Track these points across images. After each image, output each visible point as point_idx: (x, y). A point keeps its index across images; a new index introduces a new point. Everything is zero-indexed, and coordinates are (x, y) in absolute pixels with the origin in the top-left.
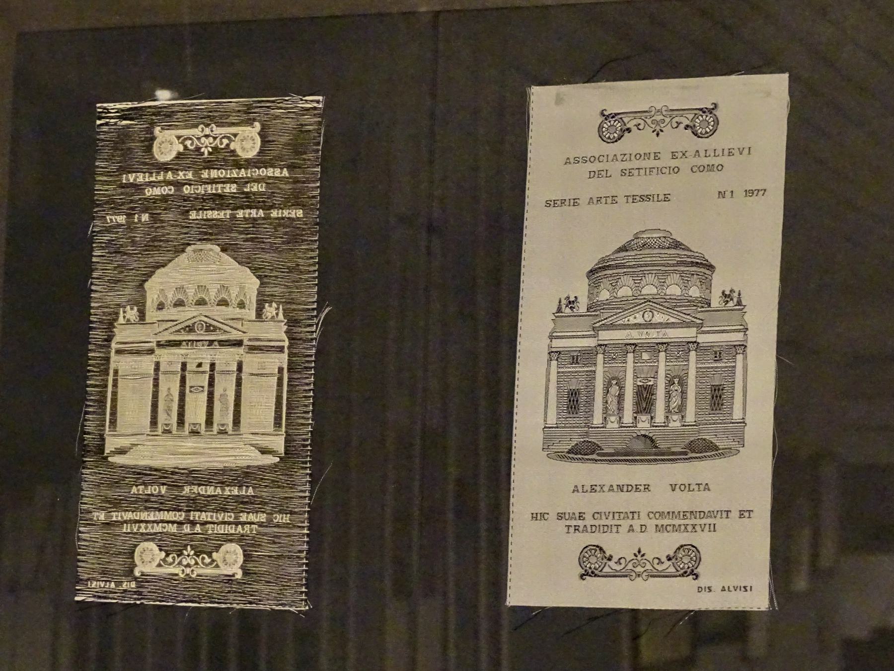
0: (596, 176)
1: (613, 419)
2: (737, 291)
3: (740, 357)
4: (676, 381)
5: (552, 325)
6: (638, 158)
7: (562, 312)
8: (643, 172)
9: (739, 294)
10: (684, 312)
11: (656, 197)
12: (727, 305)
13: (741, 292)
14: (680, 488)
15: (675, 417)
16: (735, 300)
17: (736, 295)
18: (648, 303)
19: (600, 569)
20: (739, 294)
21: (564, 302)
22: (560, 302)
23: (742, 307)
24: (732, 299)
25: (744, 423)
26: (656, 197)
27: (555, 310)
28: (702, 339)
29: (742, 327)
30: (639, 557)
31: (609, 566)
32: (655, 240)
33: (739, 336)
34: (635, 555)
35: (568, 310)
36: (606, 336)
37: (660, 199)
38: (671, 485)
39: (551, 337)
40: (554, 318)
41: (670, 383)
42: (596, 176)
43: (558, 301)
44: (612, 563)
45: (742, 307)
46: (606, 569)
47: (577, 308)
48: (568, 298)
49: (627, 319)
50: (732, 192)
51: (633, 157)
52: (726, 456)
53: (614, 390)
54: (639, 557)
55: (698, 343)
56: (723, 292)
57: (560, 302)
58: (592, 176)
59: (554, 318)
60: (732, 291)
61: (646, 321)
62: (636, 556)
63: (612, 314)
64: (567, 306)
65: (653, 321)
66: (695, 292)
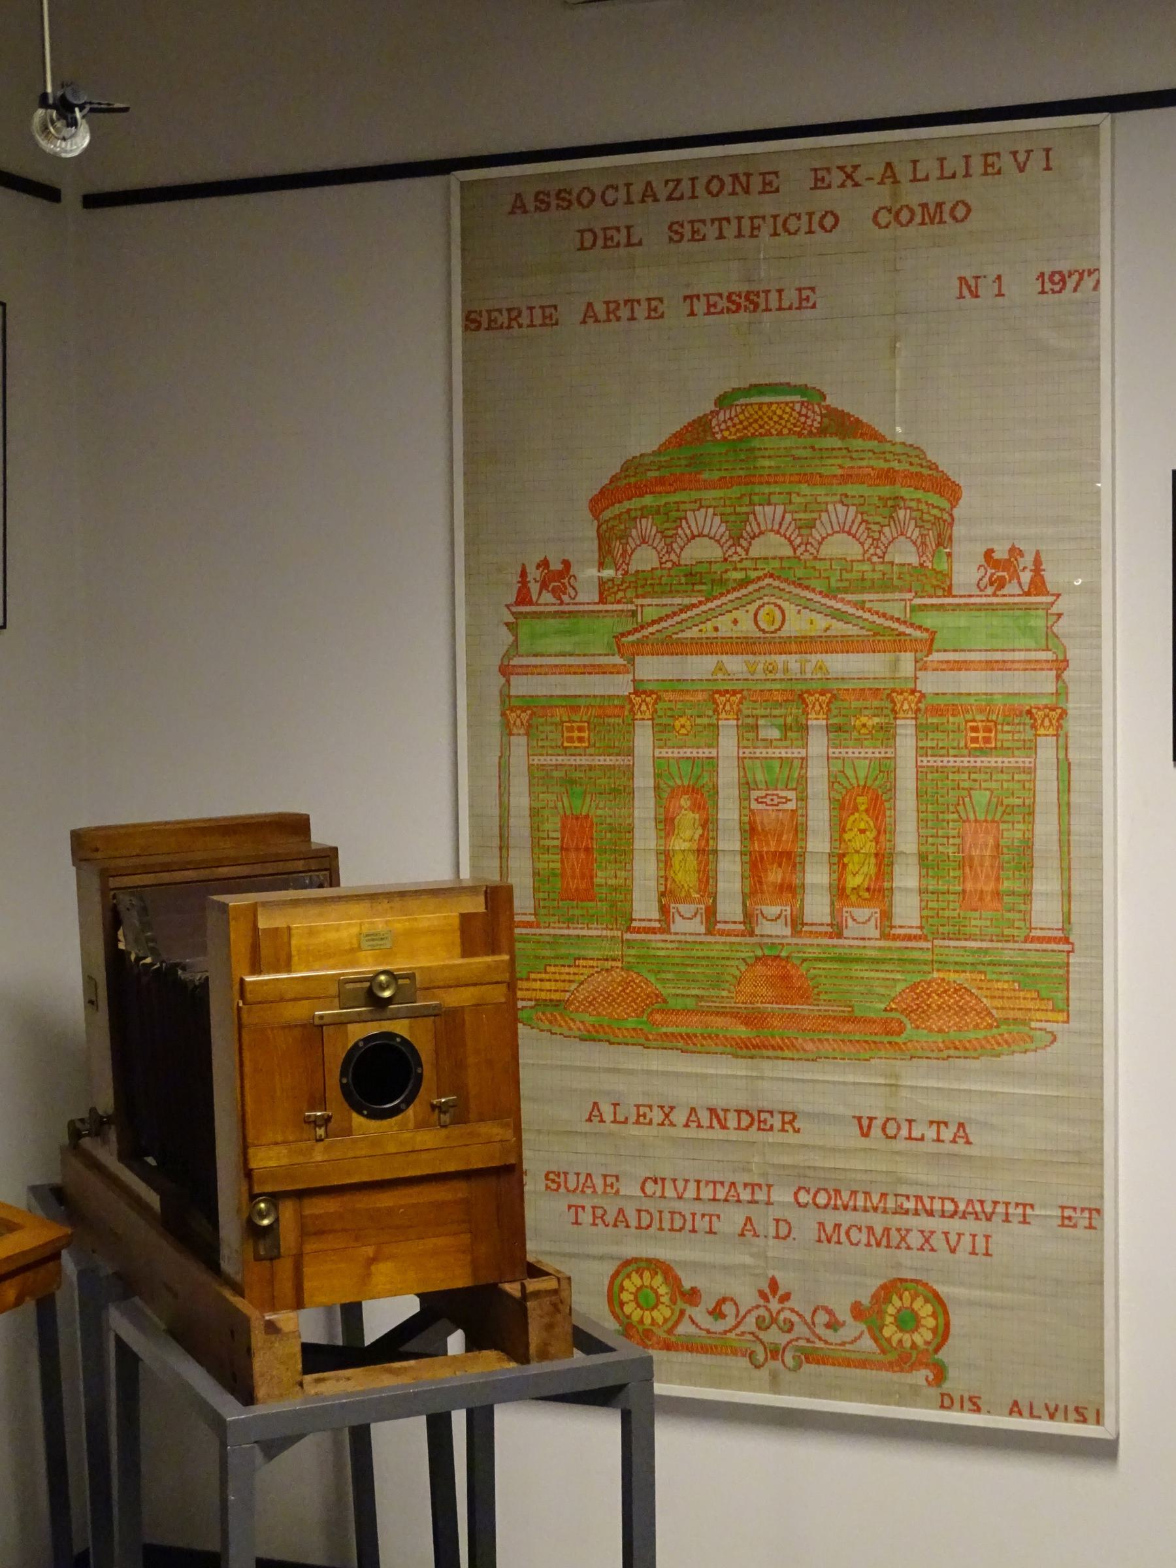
0: (600, 242)
1: (686, 909)
2: (1029, 550)
3: (1047, 751)
4: (863, 801)
5: (507, 637)
6: (715, 182)
7: (531, 603)
8: (730, 230)
9: (1037, 562)
10: (876, 606)
11: (773, 296)
12: (1004, 591)
13: (1043, 558)
14: (884, 1129)
15: (862, 913)
16: (1026, 577)
17: (1028, 561)
18: (768, 581)
19: (666, 1327)
20: (1037, 562)
21: (534, 574)
22: (524, 574)
23: (1050, 599)
24: (1015, 575)
25: (1066, 940)
26: (773, 296)
27: (512, 599)
28: (929, 683)
29: (1049, 656)
30: (774, 1305)
31: (690, 1317)
32: (779, 412)
33: (1045, 683)
34: (762, 1294)
35: (547, 597)
36: (652, 668)
37: (785, 304)
38: (859, 1119)
39: (506, 671)
40: (511, 619)
41: (842, 808)
42: (600, 242)
43: (516, 578)
44: (698, 1313)
45: (1050, 599)
46: (685, 1328)
47: (573, 594)
48: (545, 563)
49: (709, 625)
50: (999, 277)
51: (700, 190)
52: (1015, 1048)
53: (688, 820)
54: (774, 1305)
55: (923, 696)
56: (989, 554)
57: (524, 574)
58: (587, 244)
59: (511, 619)
60: (1015, 552)
61: (763, 631)
62: (767, 1300)
63: (668, 610)
64: (544, 585)
65: (786, 632)
66: (905, 554)
